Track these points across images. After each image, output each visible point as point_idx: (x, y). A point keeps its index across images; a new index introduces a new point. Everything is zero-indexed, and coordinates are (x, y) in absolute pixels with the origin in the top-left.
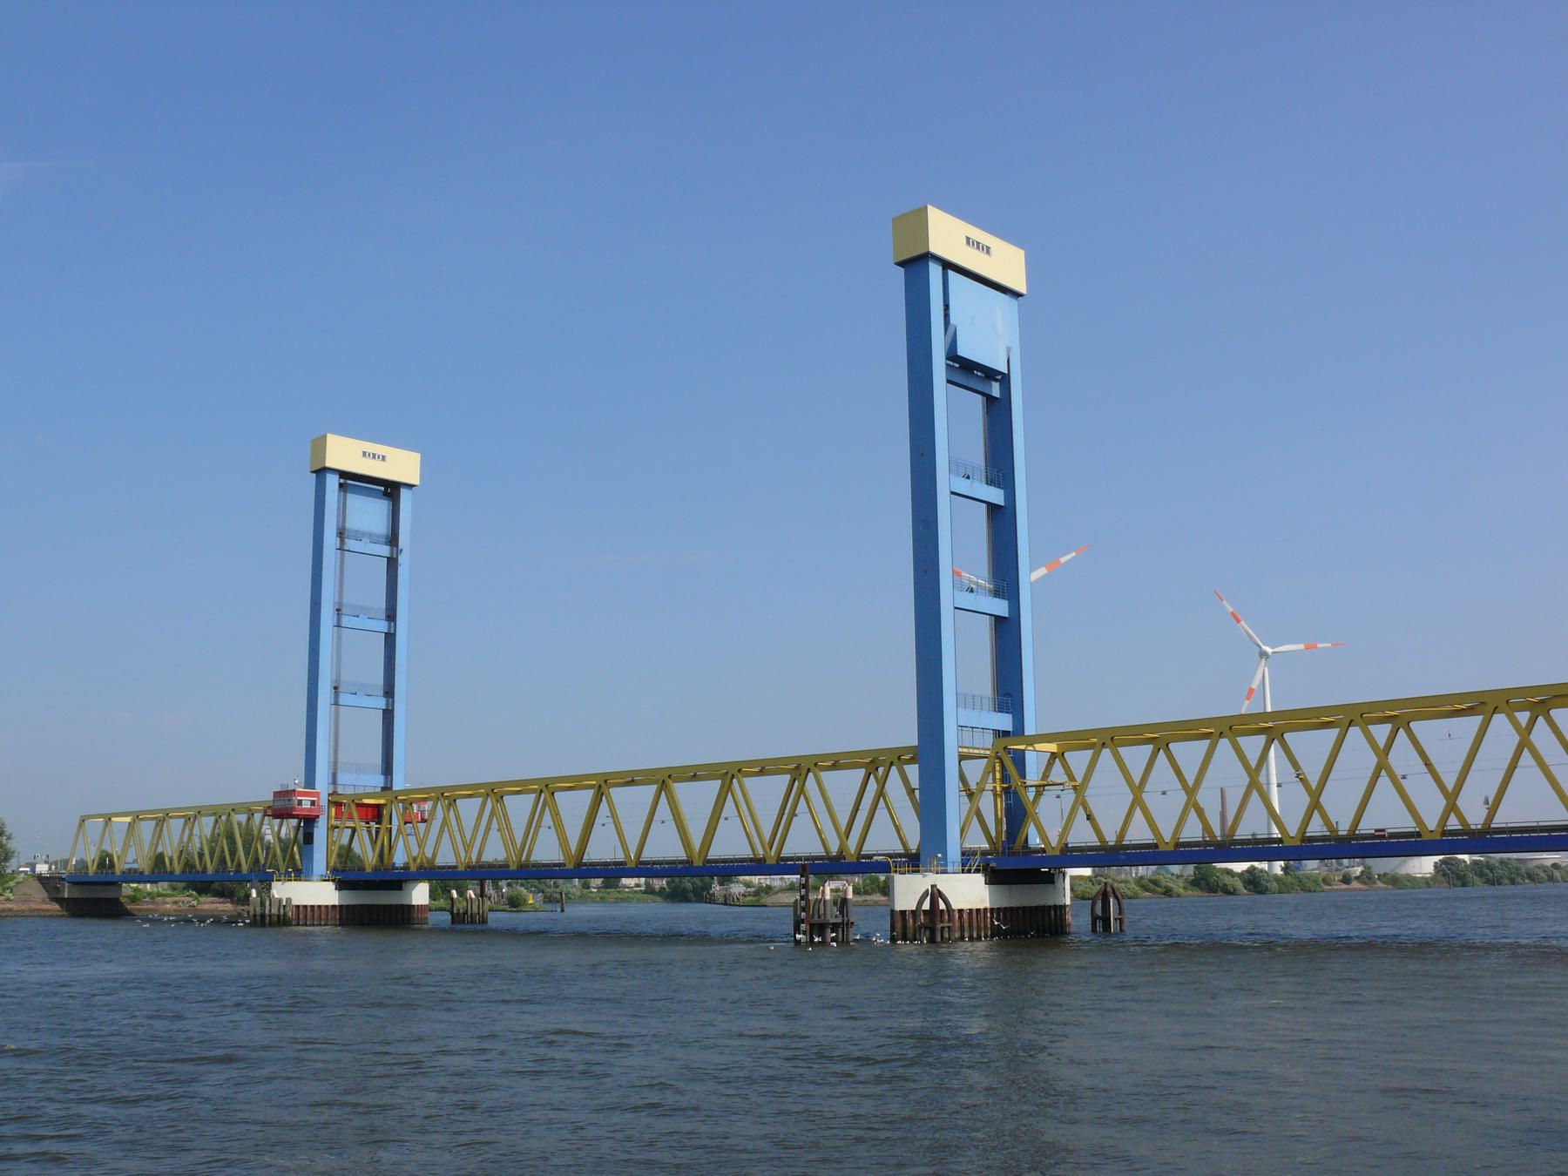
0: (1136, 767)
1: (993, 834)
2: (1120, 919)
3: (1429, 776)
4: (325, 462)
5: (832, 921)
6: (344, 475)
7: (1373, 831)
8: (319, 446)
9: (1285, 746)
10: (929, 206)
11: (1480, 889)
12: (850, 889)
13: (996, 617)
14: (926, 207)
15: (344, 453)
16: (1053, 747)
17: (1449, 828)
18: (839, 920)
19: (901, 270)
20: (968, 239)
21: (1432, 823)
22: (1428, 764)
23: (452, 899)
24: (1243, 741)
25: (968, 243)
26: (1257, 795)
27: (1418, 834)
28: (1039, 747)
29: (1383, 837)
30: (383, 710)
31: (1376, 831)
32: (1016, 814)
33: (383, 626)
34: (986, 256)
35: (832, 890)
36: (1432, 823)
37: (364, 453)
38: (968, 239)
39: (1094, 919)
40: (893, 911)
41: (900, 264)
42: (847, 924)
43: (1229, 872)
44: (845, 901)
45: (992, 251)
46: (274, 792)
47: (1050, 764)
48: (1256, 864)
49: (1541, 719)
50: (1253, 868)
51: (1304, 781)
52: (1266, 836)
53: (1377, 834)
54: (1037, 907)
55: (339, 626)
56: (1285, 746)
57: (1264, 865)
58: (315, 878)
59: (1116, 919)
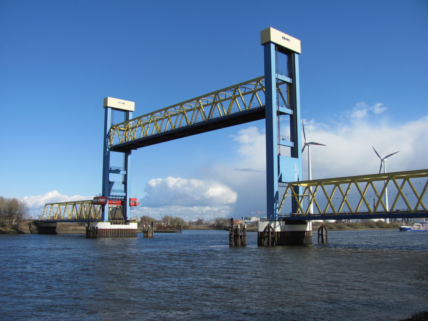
0: (399, 184)
1: (375, 205)
3: (414, 194)
4: (107, 105)
5: (240, 234)
6: (113, 108)
7: (396, 211)
8: (106, 101)
10: (271, 28)
11: (377, 229)
12: (246, 225)
13: (291, 147)
14: (270, 28)
15: (113, 102)
16: (306, 185)
18: (242, 234)
19: (263, 47)
20: (283, 37)
21: (413, 208)
23: (144, 227)
26: (401, 196)
28: (302, 185)
29: (399, 212)
30: (291, 148)
31: (397, 210)
34: (289, 42)
35: (313, 225)
36: (413, 208)
38: (283, 37)
41: (263, 45)
42: (245, 235)
43: (374, 222)
44: (244, 228)
45: (290, 41)
47: (306, 189)
49: (406, 181)
50: (381, 221)
51: (377, 195)
52: (344, 212)
53: (397, 211)
54: (301, 231)
57: (383, 220)
58: (105, 221)
59: (325, 235)
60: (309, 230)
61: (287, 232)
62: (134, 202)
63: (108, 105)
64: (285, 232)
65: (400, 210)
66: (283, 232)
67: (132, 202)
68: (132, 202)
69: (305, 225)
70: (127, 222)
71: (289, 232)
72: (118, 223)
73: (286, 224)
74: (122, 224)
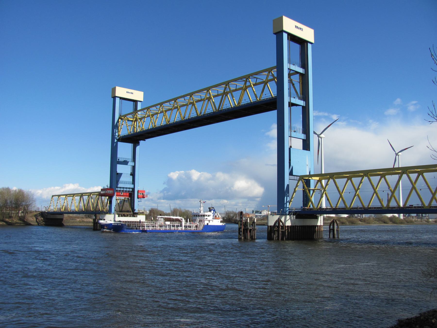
2: (338, 230)
5: (249, 228)
6: (121, 98)
7: (409, 206)
8: (114, 90)
9: (423, 177)
15: (121, 92)
16: (317, 178)
17: (432, 205)
18: (252, 228)
19: (275, 36)
20: (296, 26)
21: (426, 204)
22: (428, 186)
24: (411, 175)
25: (296, 27)
27: (382, 208)
29: (412, 208)
31: (410, 205)
32: (306, 199)
33: (303, 136)
34: (302, 31)
36: (426, 204)
37: (127, 92)
38: (296, 26)
39: (330, 229)
40: (268, 226)
41: (275, 34)
42: (254, 229)
46: (101, 189)
47: (317, 183)
48: (394, 214)
52: (356, 207)
53: (410, 206)
55: (290, 137)
56: (423, 177)
57: (396, 215)
58: (112, 213)
60: (320, 225)
61: (298, 226)
62: (142, 194)
63: (116, 95)
64: (295, 226)
65: (414, 206)
66: (293, 226)
67: (141, 194)
68: (141, 194)
69: (316, 220)
70: (135, 214)
71: (300, 226)
72: (125, 215)
73: (296, 218)
74: (130, 216)
